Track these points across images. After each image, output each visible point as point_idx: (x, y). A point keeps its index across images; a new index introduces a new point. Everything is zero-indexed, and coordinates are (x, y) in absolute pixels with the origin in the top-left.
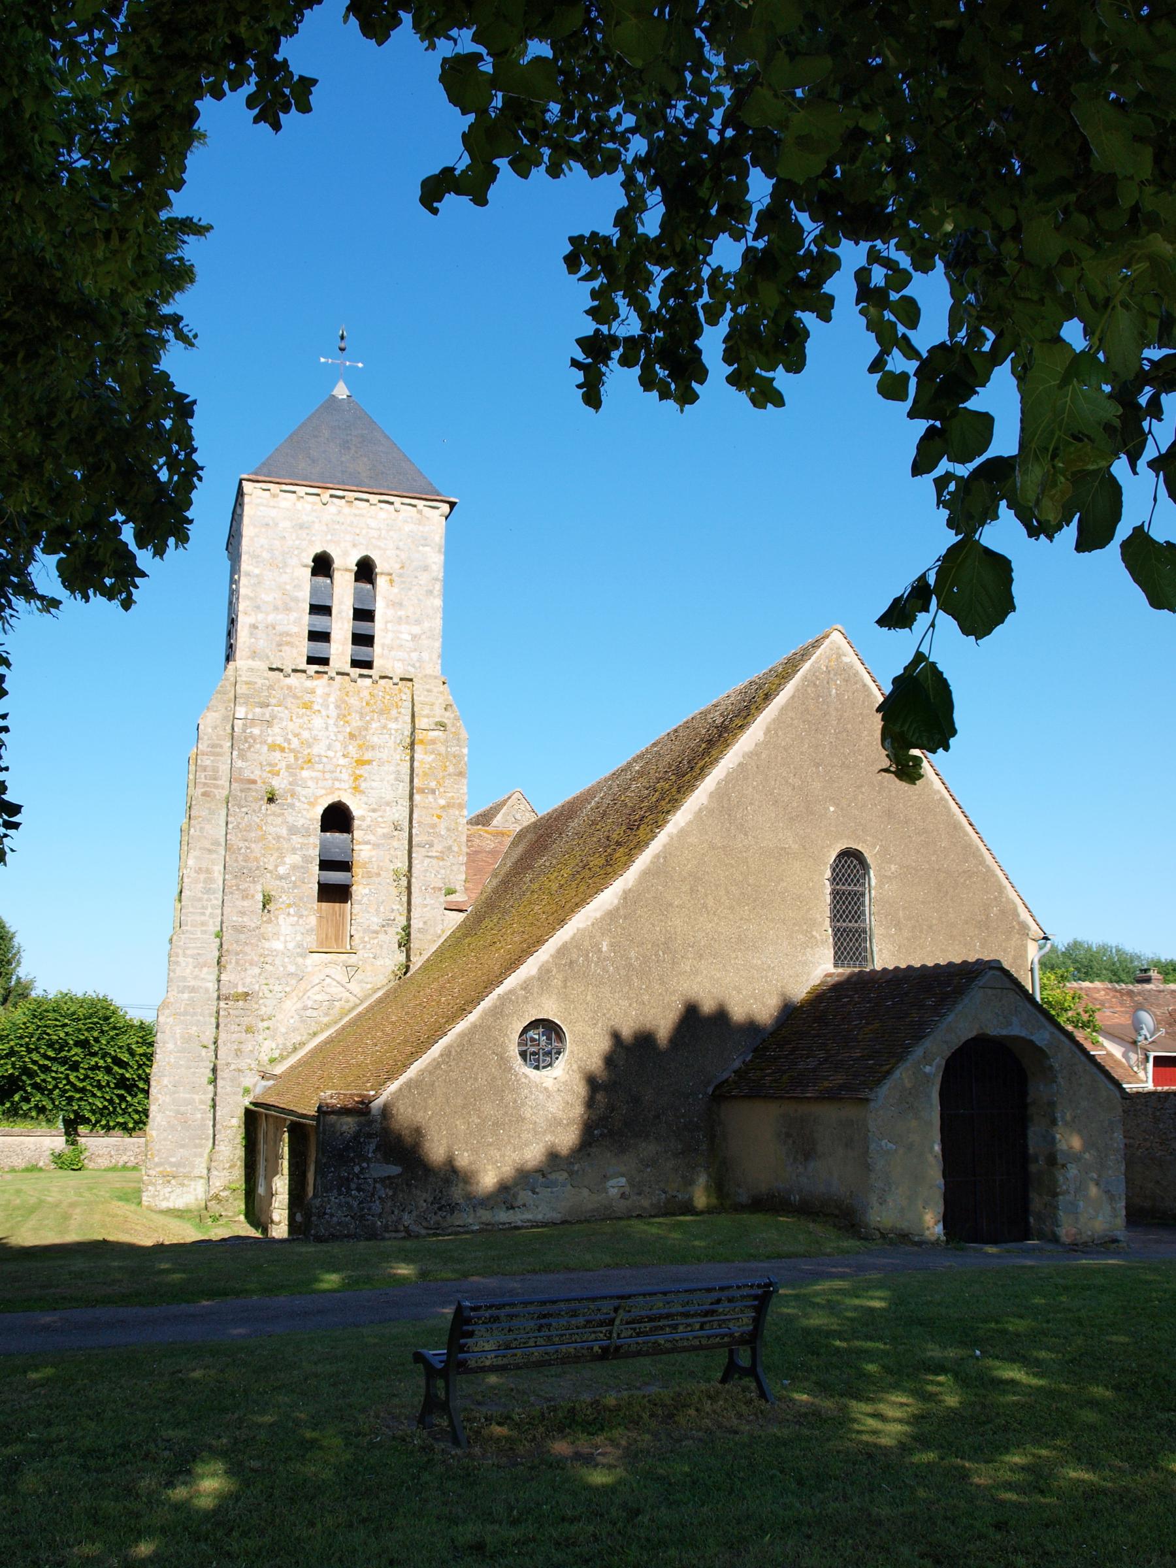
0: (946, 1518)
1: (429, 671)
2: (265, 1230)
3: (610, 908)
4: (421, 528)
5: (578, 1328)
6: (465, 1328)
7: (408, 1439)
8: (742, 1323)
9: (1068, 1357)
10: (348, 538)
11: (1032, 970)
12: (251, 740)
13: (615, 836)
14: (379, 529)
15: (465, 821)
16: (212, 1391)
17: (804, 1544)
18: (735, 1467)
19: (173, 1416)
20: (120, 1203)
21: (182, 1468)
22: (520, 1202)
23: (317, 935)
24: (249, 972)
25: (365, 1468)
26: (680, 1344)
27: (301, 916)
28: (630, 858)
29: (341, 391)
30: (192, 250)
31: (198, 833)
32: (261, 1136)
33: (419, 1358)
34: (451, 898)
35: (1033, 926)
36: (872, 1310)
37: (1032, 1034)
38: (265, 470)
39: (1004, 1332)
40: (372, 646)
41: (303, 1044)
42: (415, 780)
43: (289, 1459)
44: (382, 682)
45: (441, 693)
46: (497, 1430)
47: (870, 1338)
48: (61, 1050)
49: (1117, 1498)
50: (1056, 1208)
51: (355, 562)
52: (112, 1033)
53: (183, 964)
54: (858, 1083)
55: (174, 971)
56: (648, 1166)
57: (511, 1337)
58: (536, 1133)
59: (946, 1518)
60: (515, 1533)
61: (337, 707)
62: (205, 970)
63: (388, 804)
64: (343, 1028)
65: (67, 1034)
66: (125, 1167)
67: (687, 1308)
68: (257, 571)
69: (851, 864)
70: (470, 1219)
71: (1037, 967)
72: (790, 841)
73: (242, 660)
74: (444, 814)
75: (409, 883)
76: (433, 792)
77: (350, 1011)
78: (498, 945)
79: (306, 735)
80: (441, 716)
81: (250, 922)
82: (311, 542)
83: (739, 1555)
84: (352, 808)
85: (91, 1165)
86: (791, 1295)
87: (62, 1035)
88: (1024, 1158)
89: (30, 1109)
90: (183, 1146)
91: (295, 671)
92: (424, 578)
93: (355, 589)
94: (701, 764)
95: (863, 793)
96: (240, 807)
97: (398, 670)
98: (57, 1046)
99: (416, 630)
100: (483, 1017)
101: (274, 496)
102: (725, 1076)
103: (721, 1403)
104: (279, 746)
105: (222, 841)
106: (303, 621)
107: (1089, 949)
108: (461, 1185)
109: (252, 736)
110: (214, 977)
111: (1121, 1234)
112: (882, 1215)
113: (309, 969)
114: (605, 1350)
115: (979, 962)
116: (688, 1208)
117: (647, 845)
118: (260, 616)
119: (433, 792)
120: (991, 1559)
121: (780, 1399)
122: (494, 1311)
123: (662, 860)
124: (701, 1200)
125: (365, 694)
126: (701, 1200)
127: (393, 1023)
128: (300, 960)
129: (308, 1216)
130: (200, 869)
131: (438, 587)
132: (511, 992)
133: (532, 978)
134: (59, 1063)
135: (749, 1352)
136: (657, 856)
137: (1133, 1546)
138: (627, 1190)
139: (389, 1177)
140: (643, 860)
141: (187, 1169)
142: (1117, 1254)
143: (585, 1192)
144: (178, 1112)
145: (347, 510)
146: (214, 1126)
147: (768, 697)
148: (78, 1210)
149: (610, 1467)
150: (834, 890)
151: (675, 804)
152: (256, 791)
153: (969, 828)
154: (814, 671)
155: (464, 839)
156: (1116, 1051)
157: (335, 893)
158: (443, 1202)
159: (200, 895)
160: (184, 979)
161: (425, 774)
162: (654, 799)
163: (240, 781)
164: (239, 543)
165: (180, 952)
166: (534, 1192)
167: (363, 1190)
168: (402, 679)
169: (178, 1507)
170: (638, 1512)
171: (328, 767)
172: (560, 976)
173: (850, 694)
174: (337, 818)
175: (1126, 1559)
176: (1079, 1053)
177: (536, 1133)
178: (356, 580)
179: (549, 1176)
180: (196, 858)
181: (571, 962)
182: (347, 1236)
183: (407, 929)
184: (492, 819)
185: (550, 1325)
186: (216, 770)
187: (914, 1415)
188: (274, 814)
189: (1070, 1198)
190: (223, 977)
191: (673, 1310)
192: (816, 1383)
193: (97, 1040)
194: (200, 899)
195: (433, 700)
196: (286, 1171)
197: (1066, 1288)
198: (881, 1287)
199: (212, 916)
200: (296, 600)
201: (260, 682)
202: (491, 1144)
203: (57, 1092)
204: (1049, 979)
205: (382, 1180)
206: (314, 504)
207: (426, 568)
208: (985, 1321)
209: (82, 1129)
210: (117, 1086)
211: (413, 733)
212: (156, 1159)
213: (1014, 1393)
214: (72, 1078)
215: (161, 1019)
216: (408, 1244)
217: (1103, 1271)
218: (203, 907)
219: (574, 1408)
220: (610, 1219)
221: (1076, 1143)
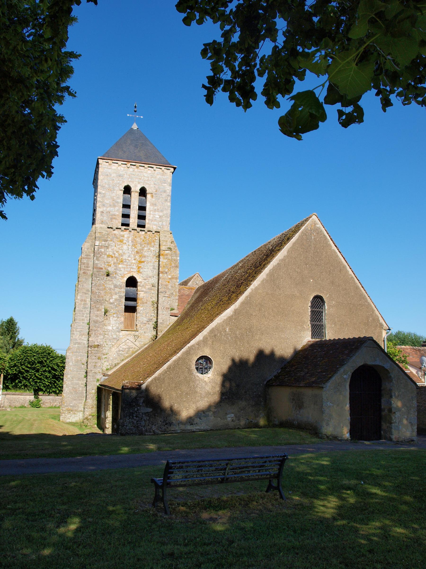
0: (350, 548)
1: (165, 229)
2: (103, 431)
3: (230, 315)
4: (163, 177)
5: (212, 471)
6: (170, 470)
7: (148, 511)
8: (275, 470)
9: (396, 485)
10: (137, 180)
11: (384, 341)
12: (101, 253)
13: (232, 290)
14: (148, 177)
15: (178, 284)
16: (77, 491)
17: (295, 557)
18: (270, 525)
19: (62, 500)
20: (52, 420)
21: (63, 521)
22: (195, 423)
23: (124, 324)
24: (99, 337)
25: (131, 522)
26: (251, 478)
27: (118, 317)
28: (237, 298)
29: (135, 127)
30: (73, 63)
32: (103, 397)
33: (153, 481)
34: (172, 312)
35: (385, 325)
36: (323, 465)
37: (384, 364)
38: (107, 155)
39: (372, 475)
40: (145, 220)
41: (118, 364)
42: (160, 269)
44: (149, 233)
45: (170, 237)
46: (182, 508)
47: (322, 476)
48: (33, 365)
49: (415, 541)
50: (391, 428)
51: (139, 189)
52: (51, 359)
53: (76, 334)
54: (319, 383)
55: (72, 337)
56: (242, 410)
57: (187, 474)
58: (201, 397)
59: (350, 548)
60: (186, 549)
61: (132, 242)
62: (83, 336)
63: (150, 277)
64: (133, 358)
65: (35, 359)
66: (55, 407)
67: (254, 464)
68: (104, 192)
69: (318, 301)
70: (178, 429)
71: (386, 340)
72: (296, 292)
73: (98, 225)
74: (170, 281)
75: (157, 306)
76: (166, 273)
77: (136, 352)
78: (189, 329)
79: (121, 252)
80: (170, 246)
81: (100, 319)
82: (123, 182)
83: (270, 561)
84: (137, 278)
85: (44, 406)
86: (293, 459)
87: (33, 359)
88: (380, 410)
89: (21, 386)
90: (75, 400)
91: (117, 228)
92: (164, 195)
93: (139, 199)
94: (264, 263)
95: (323, 275)
96: (97, 278)
97: (154, 228)
98: (31, 363)
99: (161, 214)
100: (183, 355)
101: (110, 165)
102: (270, 378)
103: (266, 500)
104: (111, 255)
105: (90, 290)
106: (120, 210)
107: (404, 334)
108: (174, 416)
109: (101, 252)
110: (86, 339)
111: (415, 438)
112: (328, 430)
113: (121, 337)
114: (223, 479)
115: (365, 337)
116: (257, 426)
117: (243, 293)
118: (105, 208)
119: (166, 273)
120: (367, 565)
121: (288, 499)
122: (181, 464)
123: (249, 298)
124: (262, 422)
125: (142, 237)
126: (262, 422)
127: (151, 357)
128: (118, 333)
129: (118, 426)
130: (82, 300)
131: (169, 198)
132: (193, 346)
133: (201, 341)
134: (32, 369)
135: (277, 481)
136: (247, 297)
137: (422, 561)
138: (234, 418)
139: (147, 413)
140: (242, 298)
141: (77, 408)
142: (414, 445)
143: (219, 419)
144: (73, 388)
145: (136, 170)
146: (86, 393)
147: (289, 239)
148: (36, 422)
149: (224, 523)
150: (311, 310)
151: (254, 278)
152: (103, 272)
153: (362, 289)
154: (306, 230)
155: (178, 290)
156: (414, 371)
157: (130, 309)
158: (167, 422)
159: (82, 309)
160: (76, 339)
161: (164, 266)
162: (246, 276)
163: (97, 268)
164: (97, 182)
165: (75, 330)
166: (200, 419)
167: (138, 417)
168: (155, 232)
169: (60, 536)
170: (233, 542)
171: (129, 264)
172: (211, 340)
173: (319, 238)
174: (132, 282)
175: (419, 566)
176: (401, 372)
177: (201, 397)
178: (139, 196)
179: (206, 413)
180: (80, 296)
181: (215, 335)
182: (132, 434)
183: (157, 322)
184: (188, 283)
185: (202, 470)
186: (88, 264)
187: (338, 506)
188: (109, 280)
189: (396, 424)
190: (90, 339)
191: (248, 465)
192: (302, 493)
193: (46, 361)
194: (82, 311)
195: (167, 239)
196: (111, 410)
198: (327, 457)
199: (86, 317)
200: (118, 203)
201: (104, 232)
202: (185, 401)
203: (31, 380)
204: (390, 344)
205: (145, 414)
206: (124, 168)
207: (165, 192)
208: (365, 470)
209: (40, 393)
210: (53, 378)
211: (159, 252)
212: (65, 404)
213: (376, 499)
214: (37, 375)
215: (68, 354)
216: (154, 437)
217: (410, 452)
218: (83, 314)
219: (211, 501)
220: (228, 429)
221: (399, 404)
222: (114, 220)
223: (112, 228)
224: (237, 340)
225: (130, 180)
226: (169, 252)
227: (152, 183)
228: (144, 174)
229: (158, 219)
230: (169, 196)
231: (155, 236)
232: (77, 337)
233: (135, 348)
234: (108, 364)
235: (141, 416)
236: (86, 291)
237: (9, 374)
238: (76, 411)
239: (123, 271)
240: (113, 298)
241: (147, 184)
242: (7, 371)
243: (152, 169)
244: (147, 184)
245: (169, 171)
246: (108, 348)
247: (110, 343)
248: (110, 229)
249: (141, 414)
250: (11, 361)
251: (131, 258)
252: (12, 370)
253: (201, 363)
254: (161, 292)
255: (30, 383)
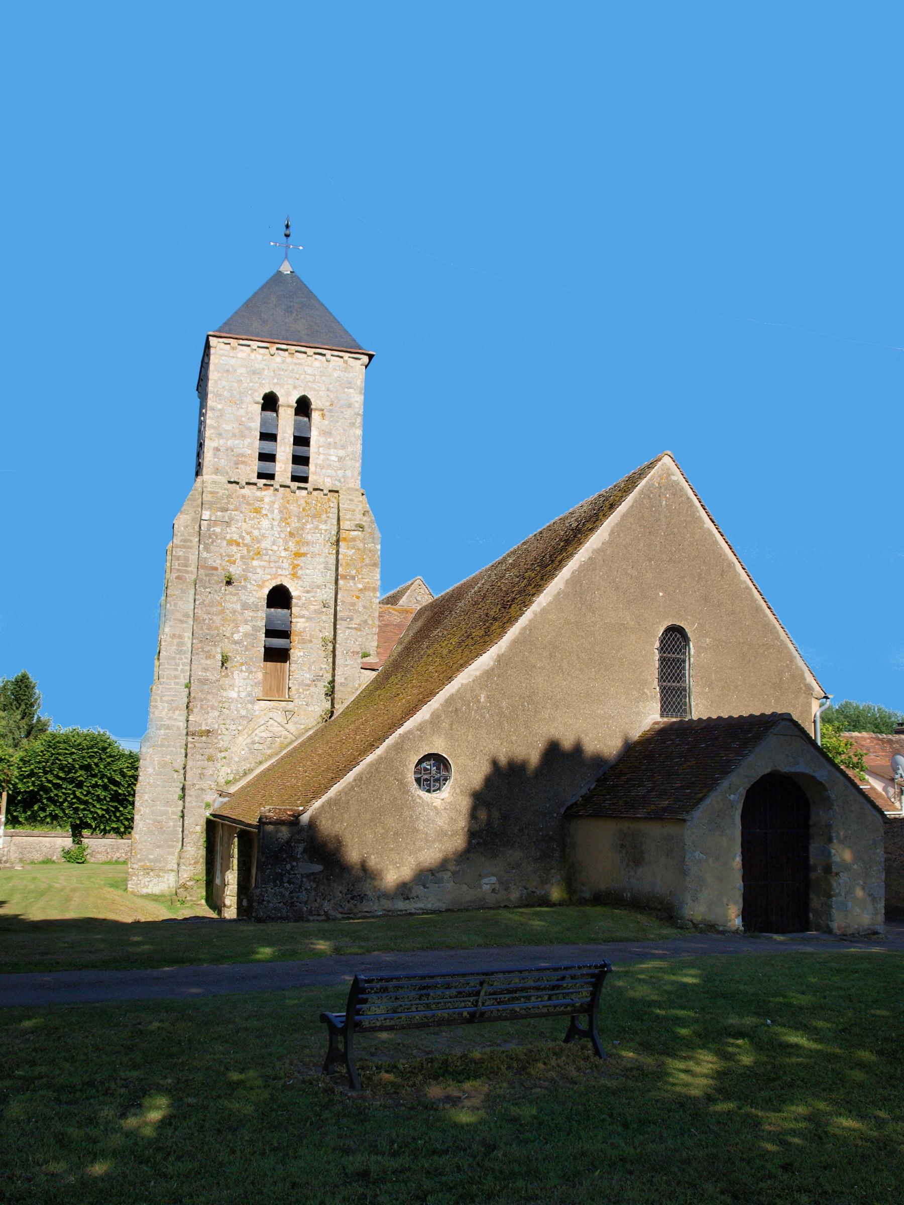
0: (742, 1160)
1: (351, 485)
2: (220, 913)
3: (487, 668)
4: (346, 375)
5: (451, 997)
6: (361, 996)
7: (314, 1083)
8: (583, 996)
9: (840, 1027)
10: (291, 381)
11: (815, 722)
12: (213, 536)
13: (492, 613)
14: (314, 375)
15: (378, 601)
16: (163, 1040)
17: (627, 1179)
18: (574, 1112)
19: (131, 1060)
20: (110, 889)
21: (134, 1103)
22: (414, 895)
23: (263, 687)
24: (211, 715)
25: (279, 1106)
26: (532, 1011)
27: (251, 672)
28: (503, 630)
29: (286, 269)
31: (173, 607)
32: (218, 840)
33: (324, 1018)
34: (365, 660)
36: (685, 985)
37: (814, 771)
38: (227, 328)
39: (789, 1005)
40: (308, 465)
41: (251, 770)
42: (340, 569)
43: (219, 1097)
44: (315, 493)
45: (361, 502)
46: (387, 1077)
48: (70, 772)
49: (881, 1145)
50: (830, 906)
51: (295, 400)
52: (108, 760)
53: (161, 708)
54: (677, 811)
56: (513, 868)
57: (396, 1004)
58: (427, 841)
59: (742, 1160)
60: (395, 1164)
61: (280, 512)
62: (177, 712)
63: (318, 587)
64: (282, 758)
65: (74, 760)
66: (117, 862)
67: (538, 983)
68: (220, 407)
69: (675, 637)
70: (377, 907)
71: (818, 720)
72: (628, 619)
73: (207, 476)
74: (361, 595)
75: (334, 648)
76: (353, 578)
77: (288, 745)
78: (401, 696)
79: (256, 533)
80: (361, 520)
81: (212, 676)
82: (262, 385)
83: (574, 1187)
84: (291, 590)
85: (92, 860)
86: (622, 972)
87: (70, 761)
88: (806, 868)
89: (46, 817)
90: (159, 847)
91: (248, 484)
92: (348, 413)
93: (295, 421)
94: (560, 558)
95: (685, 582)
96: (205, 588)
97: (328, 484)
98: (66, 769)
99: (342, 453)
100: (387, 751)
101: (234, 348)
102: (573, 800)
103: (564, 1058)
104: (235, 541)
105: (191, 614)
106: (254, 446)
109: (214, 533)
110: (184, 718)
111: (881, 928)
112: (696, 910)
113: (257, 713)
114: (472, 1015)
115: (774, 714)
116: (545, 901)
117: (516, 620)
118: (222, 441)
119: (353, 578)
120: (779, 1196)
121: (610, 1056)
122: (384, 983)
123: (528, 632)
124: (556, 893)
125: (302, 502)
126: (556, 893)
127: (319, 755)
128: (250, 706)
129: (250, 902)
130: (174, 635)
131: (359, 420)
132: (410, 732)
133: (426, 721)
134: (68, 782)
135: (587, 1018)
136: (524, 629)
137: (896, 1188)
138: (497, 886)
139: (313, 874)
140: (513, 632)
141: (162, 864)
142: (877, 943)
143: (465, 887)
144: (156, 821)
145: (289, 360)
146: (183, 832)
147: (612, 507)
148: (77, 894)
149: (475, 1109)
150: (661, 657)
151: (539, 588)
152: (218, 575)
153: (768, 611)
154: (649, 486)
155: (377, 614)
156: (878, 785)
157: (277, 655)
158: (355, 893)
159: (174, 655)
160: (161, 719)
161: (347, 564)
162: (523, 585)
163: (205, 568)
164: (206, 385)
165: (159, 698)
166: (425, 887)
167: (293, 883)
168: (330, 491)
169: (128, 1134)
170: (494, 1148)
171: (273, 558)
172: (447, 721)
173: (677, 505)
174: (279, 597)
175: (890, 1198)
176: (852, 788)
177: (427, 841)
178: (296, 414)
179: (437, 875)
180: (171, 626)
181: (456, 710)
182: (280, 918)
183: (332, 682)
184: (398, 600)
185: (429, 995)
186: (186, 559)
187: (718, 1072)
188: (231, 594)
189: (841, 899)
190: (191, 718)
191: (527, 985)
192: (640, 1044)
193: (97, 765)
194: (174, 658)
195: (355, 507)
196: (235, 867)
197: (839, 971)
198: (693, 967)
199: (183, 671)
200: (249, 429)
201: (221, 492)
202: (392, 850)
203: (66, 804)
204: (827, 729)
205: (308, 876)
206: (264, 355)
207: (350, 406)
208: (775, 996)
209: (86, 832)
210: (112, 800)
211: (338, 533)
212: (139, 856)
213: (798, 1056)
214: (78, 794)
215: (144, 750)
216: (326, 926)
217: (869, 957)
218: (176, 665)
219: (447, 1060)
220: (483, 908)
221: (848, 856)
222: (242, 466)
223: (238, 483)
224: (502, 719)
225: (275, 381)
226: (360, 533)
227: (323, 388)
228: (306, 368)
229: (335, 464)
230: (358, 414)
231: (329, 500)
232: (164, 713)
233: (286, 738)
234: (229, 771)
235: (299, 882)
236: (184, 616)
237: (20, 793)
238: (161, 870)
239: (260, 575)
240: (239, 632)
241: (312, 389)
242: (15, 785)
243: (323, 358)
244: (312, 389)
245: (359, 362)
246: (230, 738)
247: (234, 727)
248: (234, 485)
249: (299, 876)
250: (24, 764)
251: (279, 546)
252: (25, 783)
253: (427, 770)
254: (342, 619)
255: (63, 811)
